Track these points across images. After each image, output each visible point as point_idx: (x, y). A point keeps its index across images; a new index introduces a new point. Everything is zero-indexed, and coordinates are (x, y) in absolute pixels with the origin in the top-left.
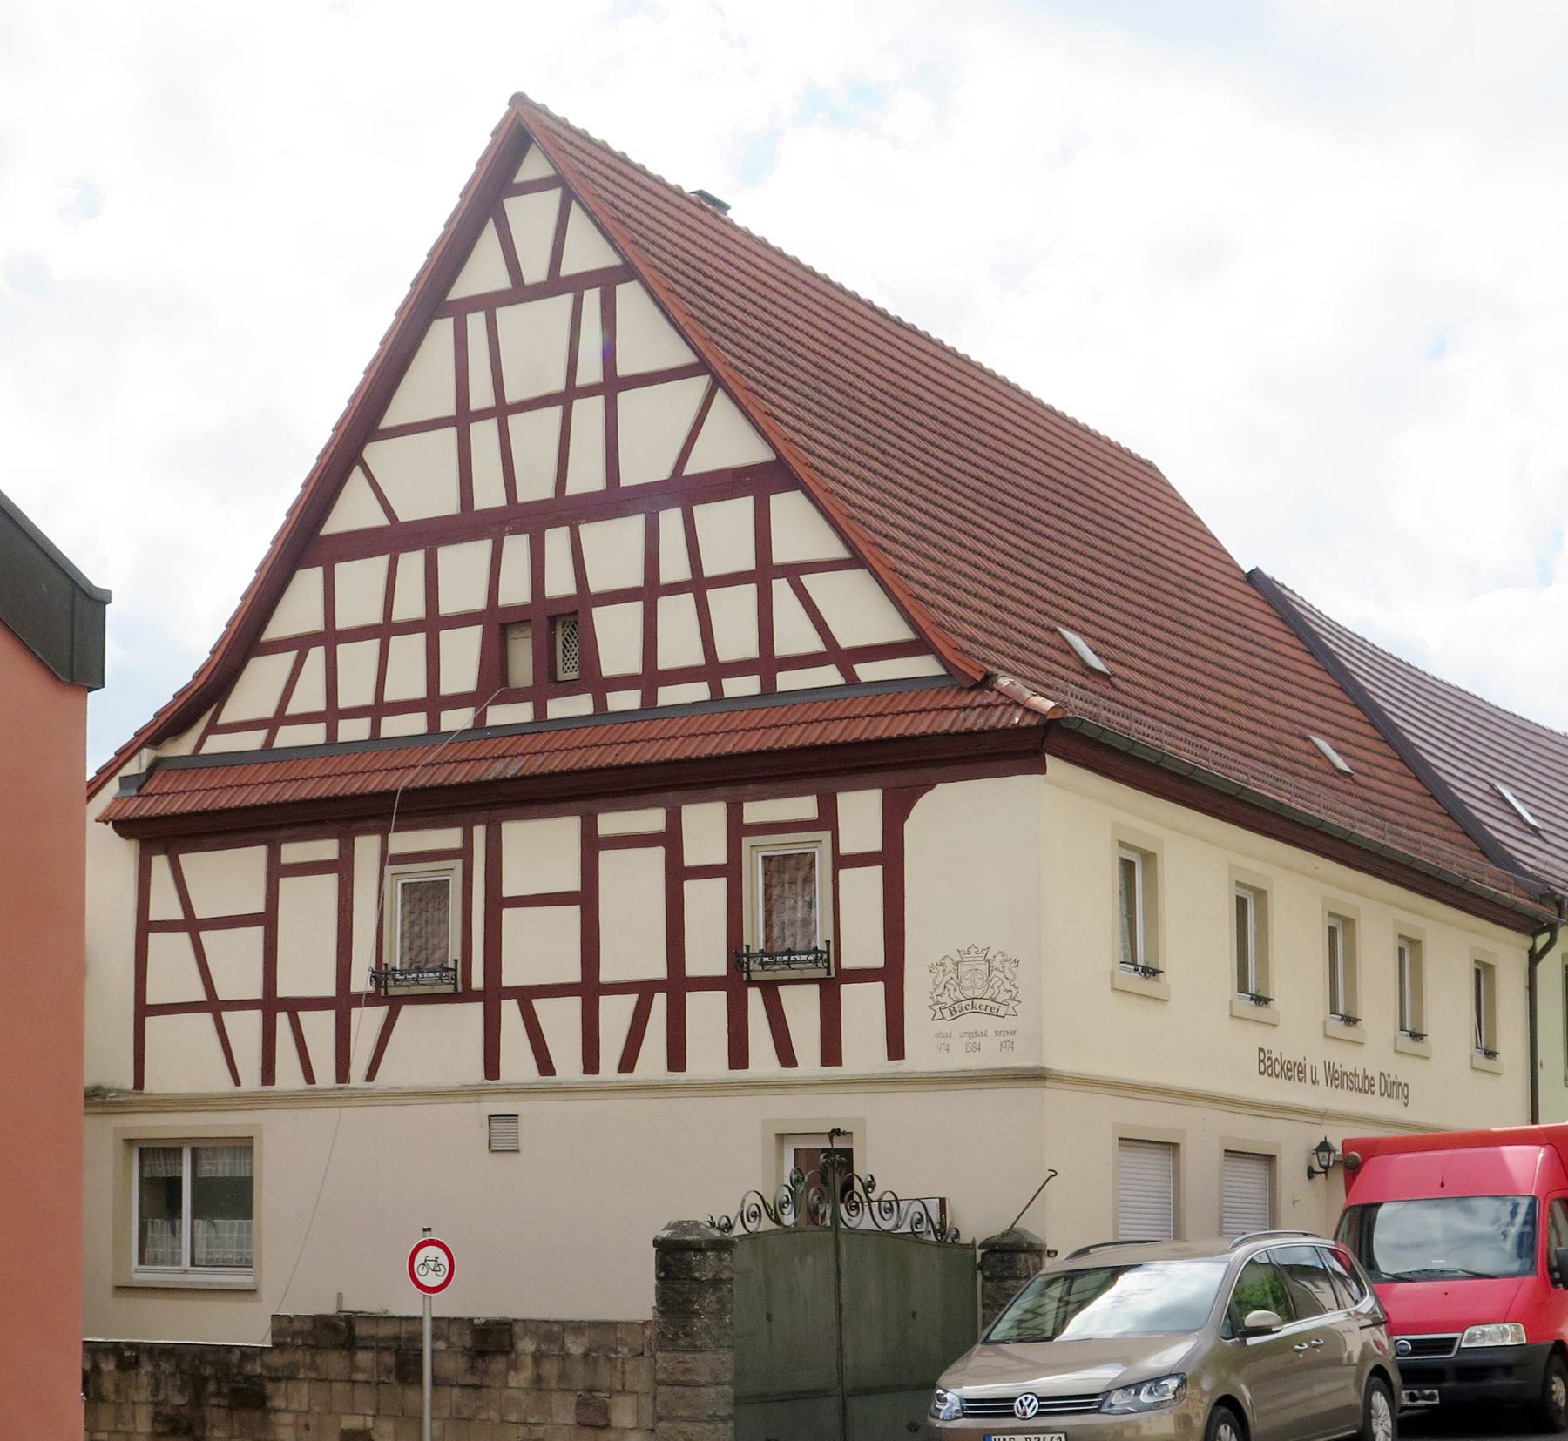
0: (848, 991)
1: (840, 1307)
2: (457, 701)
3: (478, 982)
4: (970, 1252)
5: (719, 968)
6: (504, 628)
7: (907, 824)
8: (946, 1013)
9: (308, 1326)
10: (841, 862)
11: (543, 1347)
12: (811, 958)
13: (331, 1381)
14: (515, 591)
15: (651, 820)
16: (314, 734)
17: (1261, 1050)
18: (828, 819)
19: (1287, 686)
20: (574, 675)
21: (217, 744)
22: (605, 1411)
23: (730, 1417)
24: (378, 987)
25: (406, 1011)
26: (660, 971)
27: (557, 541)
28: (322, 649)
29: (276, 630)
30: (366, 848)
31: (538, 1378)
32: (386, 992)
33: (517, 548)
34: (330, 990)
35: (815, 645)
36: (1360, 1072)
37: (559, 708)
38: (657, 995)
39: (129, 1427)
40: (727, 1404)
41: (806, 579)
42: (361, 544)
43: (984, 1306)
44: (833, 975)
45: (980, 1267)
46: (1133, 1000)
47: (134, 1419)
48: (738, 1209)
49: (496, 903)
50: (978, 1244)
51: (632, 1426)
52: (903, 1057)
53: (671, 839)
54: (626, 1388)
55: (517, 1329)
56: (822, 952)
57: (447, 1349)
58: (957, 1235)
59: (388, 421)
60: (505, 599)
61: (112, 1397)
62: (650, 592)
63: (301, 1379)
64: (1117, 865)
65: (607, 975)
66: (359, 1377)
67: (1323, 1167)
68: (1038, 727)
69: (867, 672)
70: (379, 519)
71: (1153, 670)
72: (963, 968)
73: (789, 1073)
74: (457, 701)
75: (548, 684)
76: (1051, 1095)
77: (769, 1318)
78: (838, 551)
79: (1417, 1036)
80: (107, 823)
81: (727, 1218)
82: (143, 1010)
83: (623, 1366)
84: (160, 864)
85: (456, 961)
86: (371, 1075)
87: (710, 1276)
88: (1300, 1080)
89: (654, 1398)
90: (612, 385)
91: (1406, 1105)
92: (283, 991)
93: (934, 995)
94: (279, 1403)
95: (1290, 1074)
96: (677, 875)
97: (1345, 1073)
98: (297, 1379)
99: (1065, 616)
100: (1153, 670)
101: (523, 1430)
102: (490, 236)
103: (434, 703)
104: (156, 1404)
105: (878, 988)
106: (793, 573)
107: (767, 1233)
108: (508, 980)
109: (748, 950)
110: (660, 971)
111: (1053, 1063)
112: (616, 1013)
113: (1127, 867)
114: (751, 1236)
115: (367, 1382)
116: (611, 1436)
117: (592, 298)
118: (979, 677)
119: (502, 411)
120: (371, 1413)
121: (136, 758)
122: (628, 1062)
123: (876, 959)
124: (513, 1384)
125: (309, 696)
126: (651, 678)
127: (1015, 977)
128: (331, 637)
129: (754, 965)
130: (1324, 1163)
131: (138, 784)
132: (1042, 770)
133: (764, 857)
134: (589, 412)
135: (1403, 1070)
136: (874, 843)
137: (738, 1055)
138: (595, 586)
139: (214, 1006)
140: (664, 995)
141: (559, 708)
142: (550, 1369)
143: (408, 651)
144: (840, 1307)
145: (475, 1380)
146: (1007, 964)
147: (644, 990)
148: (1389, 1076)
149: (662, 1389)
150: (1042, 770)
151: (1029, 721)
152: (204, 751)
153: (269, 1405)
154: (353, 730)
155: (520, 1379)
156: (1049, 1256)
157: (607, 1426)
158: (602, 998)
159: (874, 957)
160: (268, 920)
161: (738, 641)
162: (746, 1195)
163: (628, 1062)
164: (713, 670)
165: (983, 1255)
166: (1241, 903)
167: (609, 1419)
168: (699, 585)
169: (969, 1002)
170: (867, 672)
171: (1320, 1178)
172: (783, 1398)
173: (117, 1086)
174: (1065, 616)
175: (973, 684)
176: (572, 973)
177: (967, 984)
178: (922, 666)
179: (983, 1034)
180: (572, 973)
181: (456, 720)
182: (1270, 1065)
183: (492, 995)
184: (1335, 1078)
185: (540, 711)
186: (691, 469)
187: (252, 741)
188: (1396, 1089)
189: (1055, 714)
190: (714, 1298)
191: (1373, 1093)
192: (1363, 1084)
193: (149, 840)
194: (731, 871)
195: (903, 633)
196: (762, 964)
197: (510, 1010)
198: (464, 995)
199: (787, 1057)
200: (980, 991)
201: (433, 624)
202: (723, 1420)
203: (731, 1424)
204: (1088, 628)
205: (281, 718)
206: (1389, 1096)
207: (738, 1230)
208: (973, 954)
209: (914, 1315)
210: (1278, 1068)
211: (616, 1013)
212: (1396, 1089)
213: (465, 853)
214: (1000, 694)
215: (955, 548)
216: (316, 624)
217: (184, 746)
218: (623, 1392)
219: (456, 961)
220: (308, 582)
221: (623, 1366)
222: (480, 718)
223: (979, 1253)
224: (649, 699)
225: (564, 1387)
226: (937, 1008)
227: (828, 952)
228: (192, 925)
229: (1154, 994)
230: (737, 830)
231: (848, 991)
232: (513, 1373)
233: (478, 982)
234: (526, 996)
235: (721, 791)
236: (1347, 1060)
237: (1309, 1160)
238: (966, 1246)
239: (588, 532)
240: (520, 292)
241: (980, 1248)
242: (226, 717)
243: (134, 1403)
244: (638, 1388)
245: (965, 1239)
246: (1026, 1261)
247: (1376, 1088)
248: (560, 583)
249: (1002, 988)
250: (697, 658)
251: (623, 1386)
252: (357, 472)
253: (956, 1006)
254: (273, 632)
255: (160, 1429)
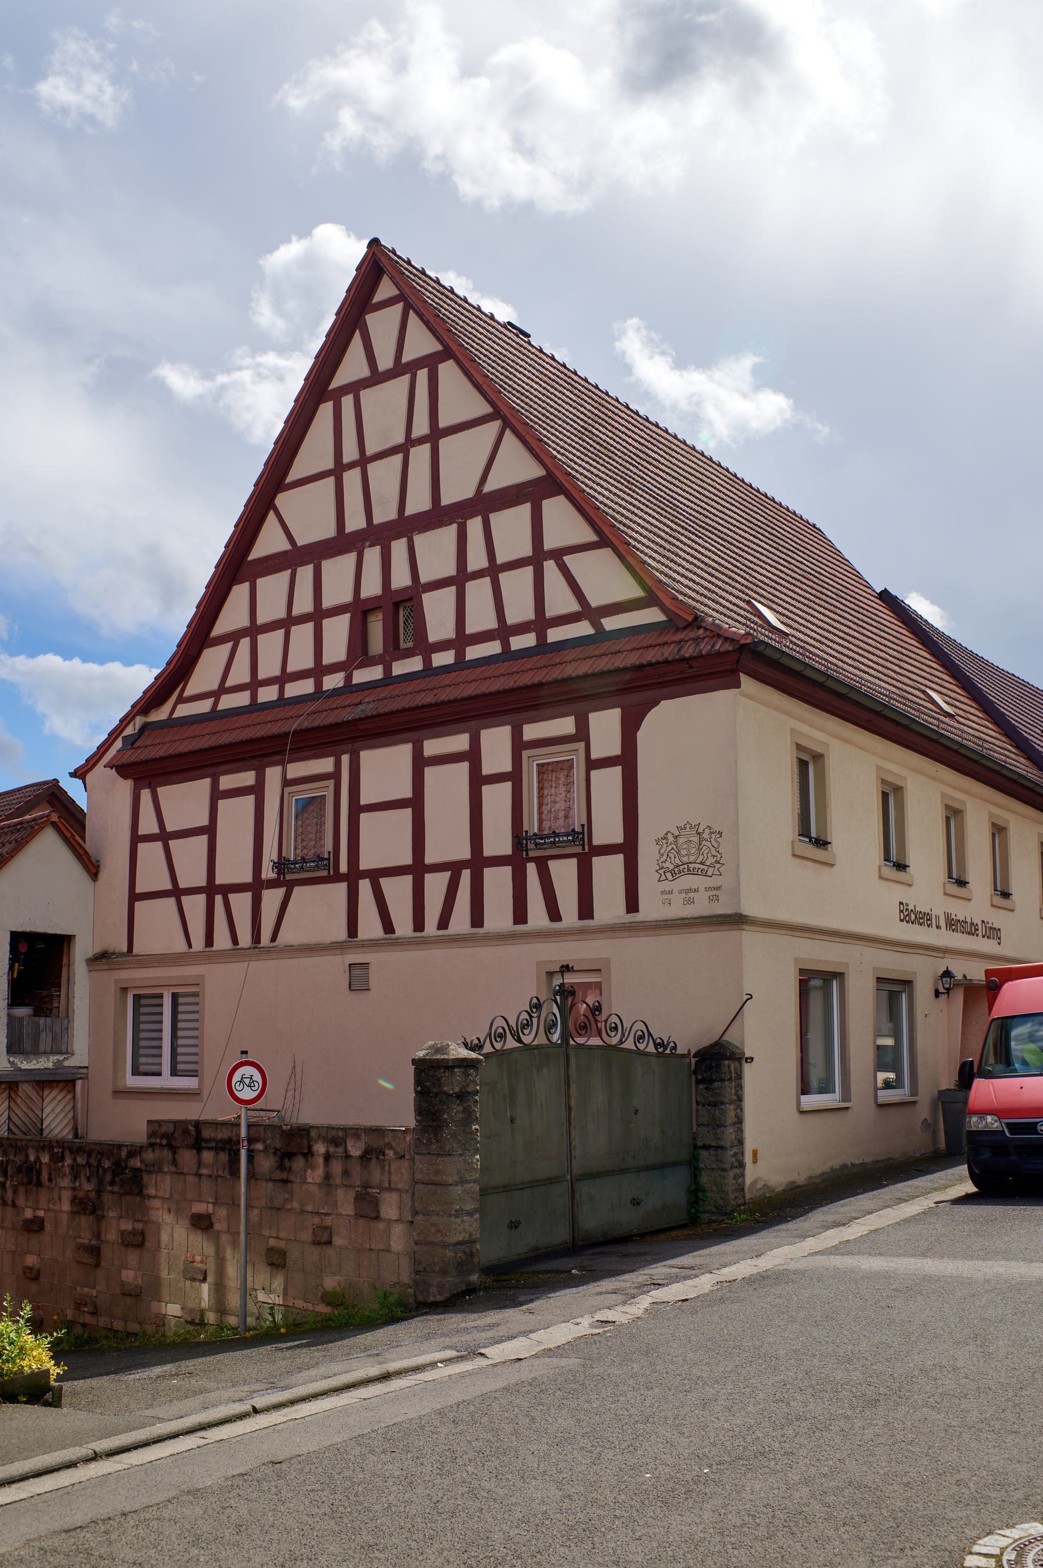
0: (597, 862)
1: (569, 1109)
2: (334, 668)
3: (343, 868)
4: (687, 1060)
5: (506, 849)
6: (365, 613)
7: (639, 734)
8: (669, 875)
9: (171, 1129)
10: (592, 764)
11: (332, 1149)
12: (570, 838)
13: (185, 1174)
14: (372, 588)
15: (460, 742)
16: (243, 699)
17: (901, 903)
18: (582, 734)
19: (908, 659)
20: (411, 644)
21: (184, 710)
22: (375, 1204)
23: (476, 1210)
24: (279, 873)
25: (297, 890)
26: (466, 854)
27: (399, 548)
28: (248, 638)
29: (220, 628)
30: (273, 775)
31: (327, 1177)
32: (284, 878)
33: (373, 555)
34: (248, 878)
35: (574, 607)
36: (969, 920)
37: (400, 668)
38: (464, 872)
39: (57, 1207)
40: (473, 1199)
41: (567, 559)
42: (273, 564)
43: (698, 1103)
44: (587, 850)
45: (695, 1072)
46: (809, 864)
47: (60, 1199)
48: (487, 1031)
49: (357, 809)
50: (692, 1054)
51: (396, 1218)
52: (637, 911)
53: (473, 756)
54: (392, 1186)
55: (313, 1134)
56: (578, 833)
57: (263, 1151)
58: (675, 1048)
59: (291, 477)
60: (364, 594)
61: (47, 1183)
62: (461, 579)
63: (165, 1172)
64: (795, 760)
65: (429, 859)
66: (204, 1171)
67: (946, 989)
68: (734, 651)
69: (610, 623)
70: (284, 546)
71: (818, 637)
72: (681, 840)
73: (557, 925)
74: (334, 668)
75: (394, 651)
76: (748, 937)
77: (512, 1121)
78: (591, 537)
79: (1006, 895)
80: (112, 768)
81: (478, 1038)
82: (134, 897)
83: (389, 1166)
84: (146, 795)
85: (329, 852)
86: (274, 938)
87: (457, 1089)
88: (929, 926)
89: (413, 1194)
90: (436, 434)
91: (999, 944)
92: (219, 881)
93: (660, 861)
94: (152, 1191)
95: (921, 921)
96: (478, 781)
97: (959, 921)
98: (162, 1172)
99: (756, 596)
100: (818, 637)
101: (316, 1220)
102: (357, 340)
103: (319, 671)
104: (74, 1189)
105: (619, 859)
106: (558, 555)
107: (513, 1050)
108: (363, 866)
109: (526, 834)
110: (466, 854)
111: (749, 909)
112: (436, 885)
113: (803, 765)
114: (500, 1054)
115: (210, 1176)
116: (381, 1226)
117: (423, 375)
118: (690, 618)
119: (364, 461)
120: (211, 1200)
121: (131, 725)
122: (444, 922)
123: (618, 838)
124: (310, 1180)
125: (240, 674)
126: (462, 640)
127: (719, 846)
128: (254, 630)
129: (531, 846)
130: (947, 986)
131: (131, 742)
132: (737, 685)
133: (538, 765)
134: (421, 455)
135: (997, 919)
136: (616, 750)
137: (520, 915)
138: (424, 578)
139: (176, 892)
140: (469, 871)
141: (400, 668)
142: (337, 1167)
143: (302, 634)
144: (569, 1109)
145: (284, 1176)
146: (713, 836)
147: (454, 868)
148: (988, 923)
149: (419, 1187)
150: (737, 685)
151: (728, 647)
152: (175, 716)
153: (145, 1192)
154: (268, 694)
155: (315, 1176)
156: (747, 1062)
157: (377, 1218)
158: (426, 875)
159: (617, 837)
160: (210, 830)
161: (520, 609)
162: (494, 1020)
163: (444, 922)
164: (504, 631)
165: (696, 1062)
166: (885, 796)
167: (378, 1212)
168: (494, 570)
169: (686, 866)
170: (610, 623)
171: (943, 997)
172: (523, 1187)
173: (117, 951)
174: (756, 596)
175: (686, 623)
176: (406, 858)
177: (684, 852)
178: (652, 615)
179: (696, 891)
180: (406, 858)
181: (333, 682)
182: (909, 915)
183: (353, 877)
184: (953, 924)
185: (388, 670)
186: (488, 488)
187: (204, 707)
188: (993, 933)
189: (746, 640)
190: (460, 1108)
191: (977, 935)
192: (970, 929)
193: (140, 778)
194: (514, 777)
195: (637, 592)
196: (536, 844)
197: (365, 886)
198: (335, 878)
199: (554, 915)
200: (694, 857)
201: (318, 615)
202: (470, 1214)
203: (477, 1216)
204: (774, 606)
205: (223, 690)
206: (988, 938)
207: (488, 1049)
208: (688, 829)
209: (636, 1112)
210: (913, 917)
211: (436, 885)
212: (993, 933)
213: (336, 775)
214: (706, 629)
215: (678, 543)
216: (244, 622)
217: (161, 714)
218: (390, 1189)
219: (329, 852)
220: (240, 592)
221: (389, 1166)
222: (349, 678)
223: (693, 1060)
224: (460, 655)
225: (345, 1183)
226: (661, 871)
227: (583, 833)
228: (164, 837)
229: (823, 860)
230: (519, 745)
231: (597, 862)
232: (309, 1171)
233: (343, 868)
234: (375, 875)
235: (507, 717)
236: (961, 911)
237: (936, 983)
238: (683, 1056)
239: (419, 540)
240: (376, 378)
241: (694, 1056)
242: (187, 693)
243: (60, 1188)
244: (400, 1186)
245: (681, 1050)
246: (729, 1067)
247: (980, 932)
248: (401, 579)
249: (710, 855)
250: (492, 623)
251: (390, 1183)
252: (271, 514)
253: (676, 870)
254: (217, 630)
255: (75, 1209)
